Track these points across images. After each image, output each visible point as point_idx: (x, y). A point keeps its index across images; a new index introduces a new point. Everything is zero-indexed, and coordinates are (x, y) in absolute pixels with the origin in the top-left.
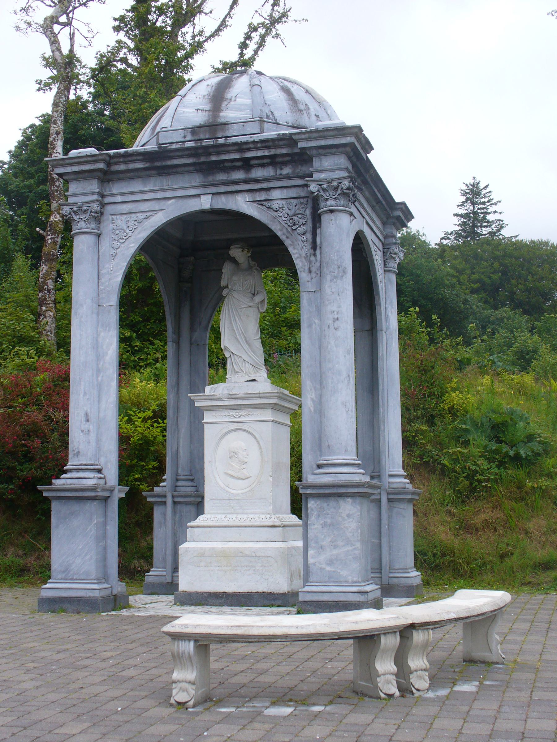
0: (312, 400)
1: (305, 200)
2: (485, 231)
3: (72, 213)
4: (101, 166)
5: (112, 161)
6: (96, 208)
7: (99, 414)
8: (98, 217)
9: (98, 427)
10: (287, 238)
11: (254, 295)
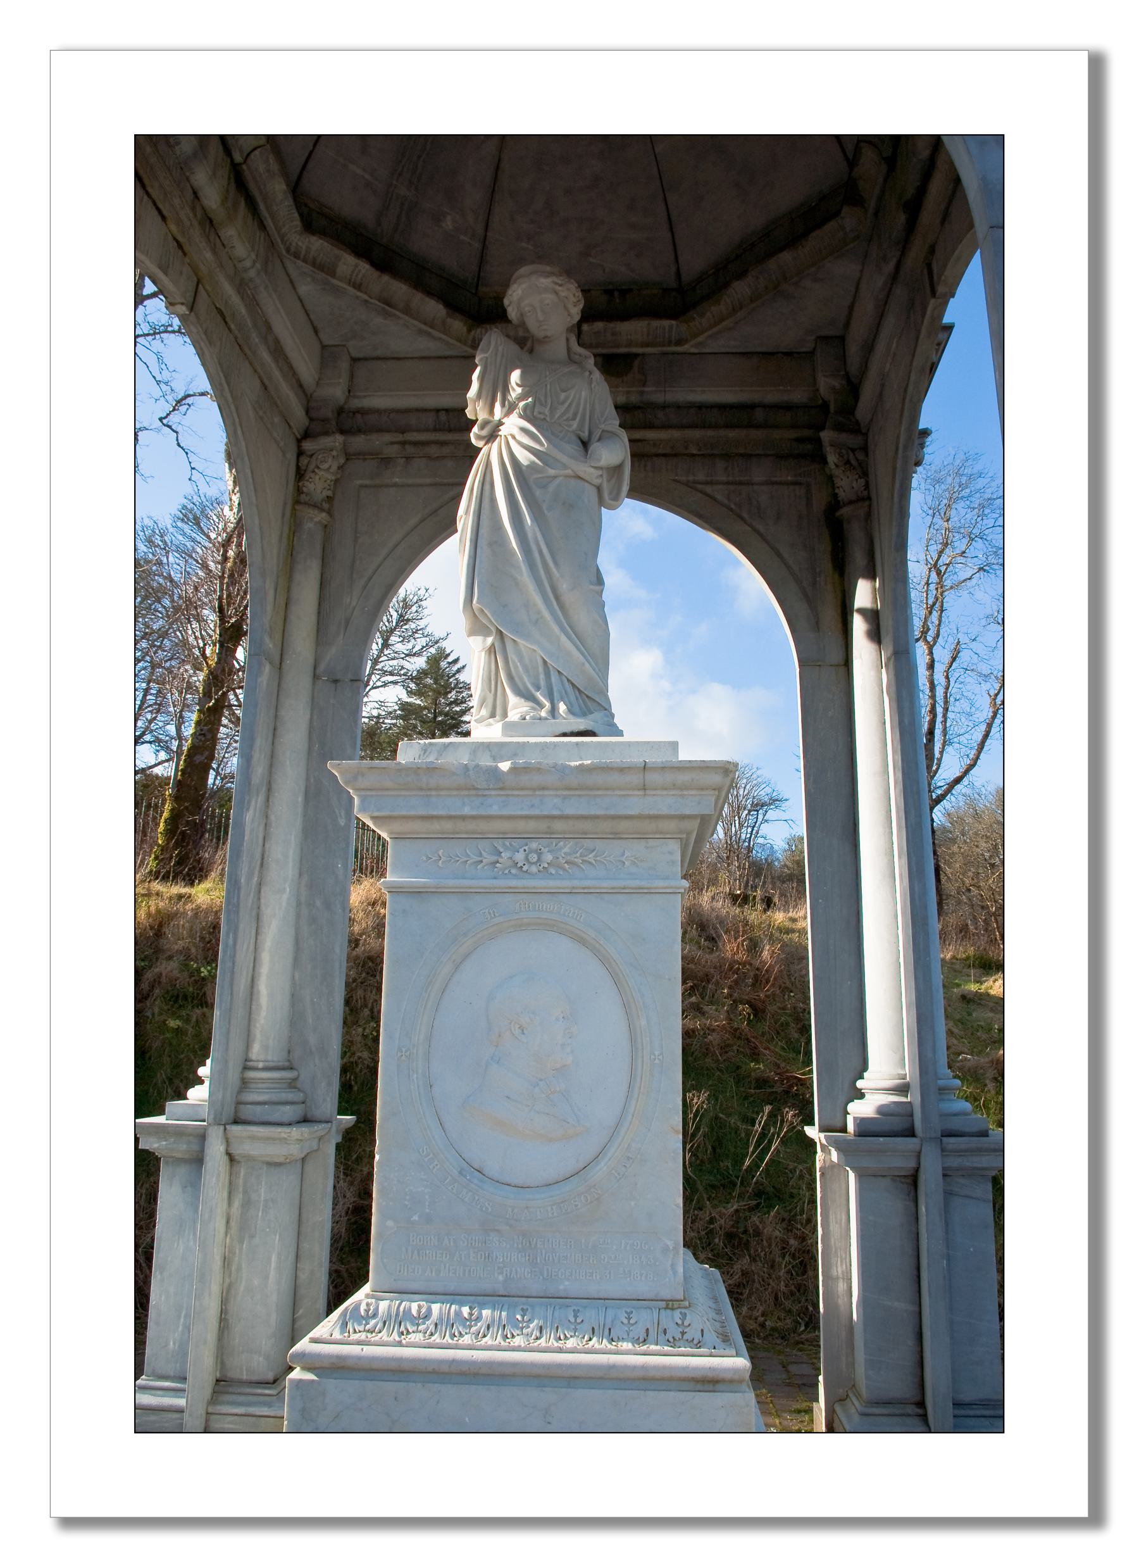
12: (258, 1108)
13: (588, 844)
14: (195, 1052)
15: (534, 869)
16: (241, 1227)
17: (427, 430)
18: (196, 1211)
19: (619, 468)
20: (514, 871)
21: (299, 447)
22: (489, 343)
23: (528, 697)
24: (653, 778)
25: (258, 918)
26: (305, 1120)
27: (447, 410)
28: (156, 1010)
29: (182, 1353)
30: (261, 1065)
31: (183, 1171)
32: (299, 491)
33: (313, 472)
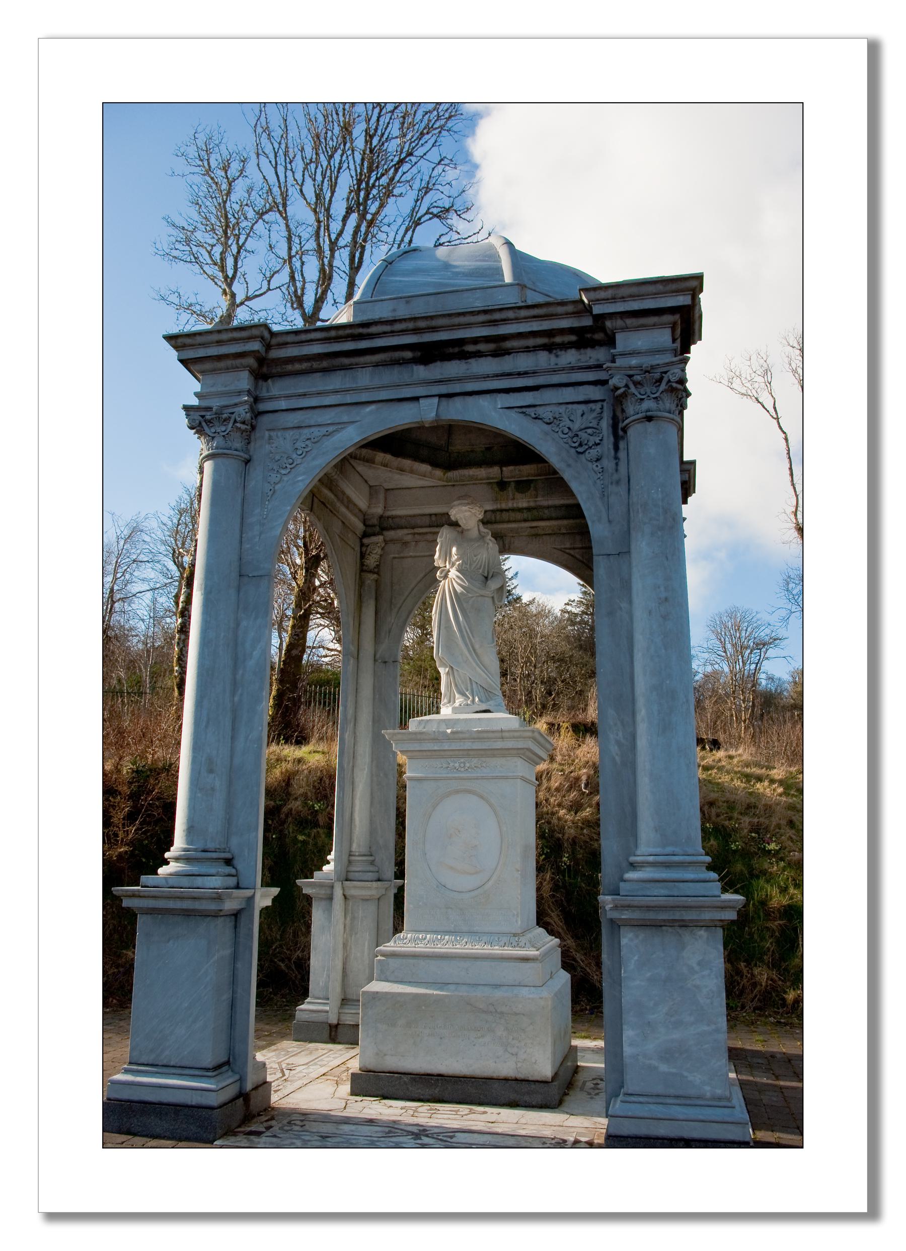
0: (618, 743)
1: (599, 405)
3: (204, 424)
4: (256, 346)
5: (274, 341)
6: (243, 415)
8: (246, 430)
9: (230, 783)
11: (486, 578)
12: (357, 874)
13: (484, 759)
14: (315, 854)
16: (350, 929)
17: (426, 527)
18: (330, 922)
21: (361, 542)
23: (463, 694)
24: (505, 734)
25: (353, 783)
26: (379, 880)
27: (436, 515)
28: (291, 830)
29: (326, 988)
31: (323, 903)
32: (362, 564)
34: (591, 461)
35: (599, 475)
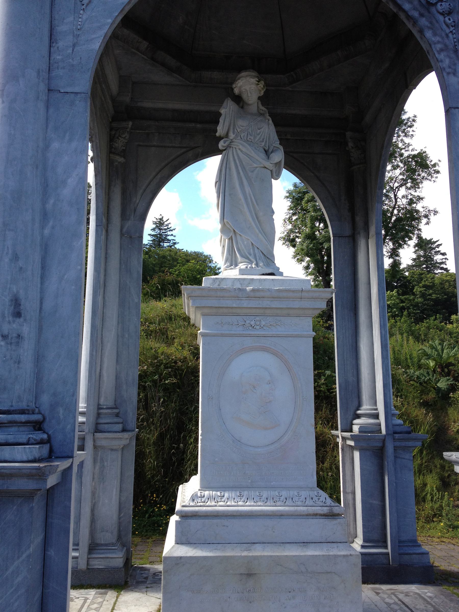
2: (166, 245)
7: (41, 303)
9: (40, 329)
10: (422, 15)
12: (106, 426)
15: (258, 327)
19: (280, 162)
20: (250, 328)
22: (227, 104)
30: (105, 407)
33: (118, 138)
34: (442, 14)
35: (452, 29)
